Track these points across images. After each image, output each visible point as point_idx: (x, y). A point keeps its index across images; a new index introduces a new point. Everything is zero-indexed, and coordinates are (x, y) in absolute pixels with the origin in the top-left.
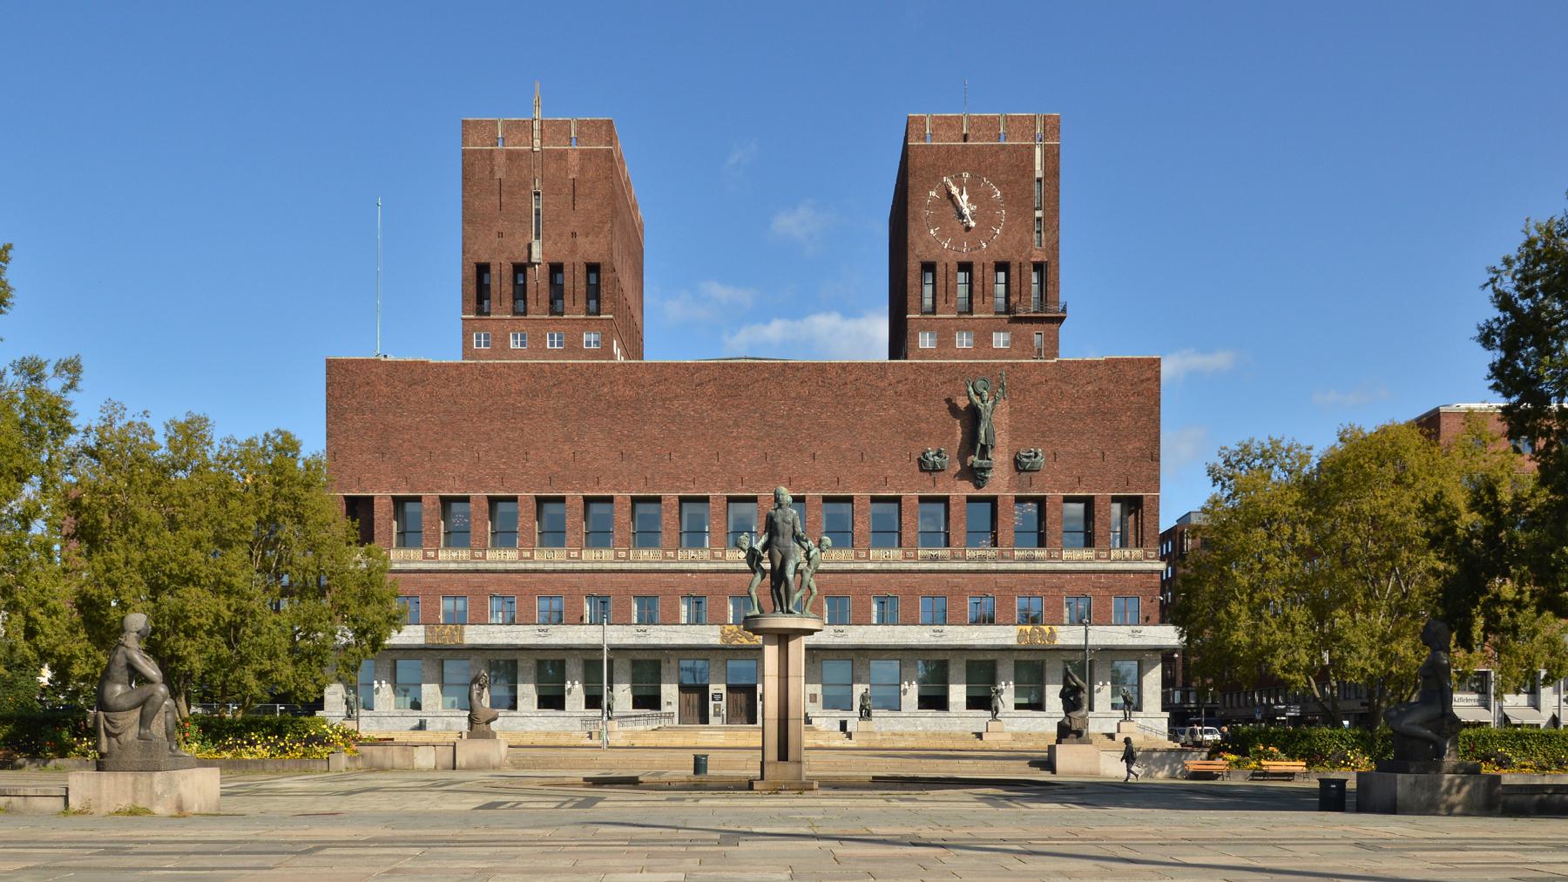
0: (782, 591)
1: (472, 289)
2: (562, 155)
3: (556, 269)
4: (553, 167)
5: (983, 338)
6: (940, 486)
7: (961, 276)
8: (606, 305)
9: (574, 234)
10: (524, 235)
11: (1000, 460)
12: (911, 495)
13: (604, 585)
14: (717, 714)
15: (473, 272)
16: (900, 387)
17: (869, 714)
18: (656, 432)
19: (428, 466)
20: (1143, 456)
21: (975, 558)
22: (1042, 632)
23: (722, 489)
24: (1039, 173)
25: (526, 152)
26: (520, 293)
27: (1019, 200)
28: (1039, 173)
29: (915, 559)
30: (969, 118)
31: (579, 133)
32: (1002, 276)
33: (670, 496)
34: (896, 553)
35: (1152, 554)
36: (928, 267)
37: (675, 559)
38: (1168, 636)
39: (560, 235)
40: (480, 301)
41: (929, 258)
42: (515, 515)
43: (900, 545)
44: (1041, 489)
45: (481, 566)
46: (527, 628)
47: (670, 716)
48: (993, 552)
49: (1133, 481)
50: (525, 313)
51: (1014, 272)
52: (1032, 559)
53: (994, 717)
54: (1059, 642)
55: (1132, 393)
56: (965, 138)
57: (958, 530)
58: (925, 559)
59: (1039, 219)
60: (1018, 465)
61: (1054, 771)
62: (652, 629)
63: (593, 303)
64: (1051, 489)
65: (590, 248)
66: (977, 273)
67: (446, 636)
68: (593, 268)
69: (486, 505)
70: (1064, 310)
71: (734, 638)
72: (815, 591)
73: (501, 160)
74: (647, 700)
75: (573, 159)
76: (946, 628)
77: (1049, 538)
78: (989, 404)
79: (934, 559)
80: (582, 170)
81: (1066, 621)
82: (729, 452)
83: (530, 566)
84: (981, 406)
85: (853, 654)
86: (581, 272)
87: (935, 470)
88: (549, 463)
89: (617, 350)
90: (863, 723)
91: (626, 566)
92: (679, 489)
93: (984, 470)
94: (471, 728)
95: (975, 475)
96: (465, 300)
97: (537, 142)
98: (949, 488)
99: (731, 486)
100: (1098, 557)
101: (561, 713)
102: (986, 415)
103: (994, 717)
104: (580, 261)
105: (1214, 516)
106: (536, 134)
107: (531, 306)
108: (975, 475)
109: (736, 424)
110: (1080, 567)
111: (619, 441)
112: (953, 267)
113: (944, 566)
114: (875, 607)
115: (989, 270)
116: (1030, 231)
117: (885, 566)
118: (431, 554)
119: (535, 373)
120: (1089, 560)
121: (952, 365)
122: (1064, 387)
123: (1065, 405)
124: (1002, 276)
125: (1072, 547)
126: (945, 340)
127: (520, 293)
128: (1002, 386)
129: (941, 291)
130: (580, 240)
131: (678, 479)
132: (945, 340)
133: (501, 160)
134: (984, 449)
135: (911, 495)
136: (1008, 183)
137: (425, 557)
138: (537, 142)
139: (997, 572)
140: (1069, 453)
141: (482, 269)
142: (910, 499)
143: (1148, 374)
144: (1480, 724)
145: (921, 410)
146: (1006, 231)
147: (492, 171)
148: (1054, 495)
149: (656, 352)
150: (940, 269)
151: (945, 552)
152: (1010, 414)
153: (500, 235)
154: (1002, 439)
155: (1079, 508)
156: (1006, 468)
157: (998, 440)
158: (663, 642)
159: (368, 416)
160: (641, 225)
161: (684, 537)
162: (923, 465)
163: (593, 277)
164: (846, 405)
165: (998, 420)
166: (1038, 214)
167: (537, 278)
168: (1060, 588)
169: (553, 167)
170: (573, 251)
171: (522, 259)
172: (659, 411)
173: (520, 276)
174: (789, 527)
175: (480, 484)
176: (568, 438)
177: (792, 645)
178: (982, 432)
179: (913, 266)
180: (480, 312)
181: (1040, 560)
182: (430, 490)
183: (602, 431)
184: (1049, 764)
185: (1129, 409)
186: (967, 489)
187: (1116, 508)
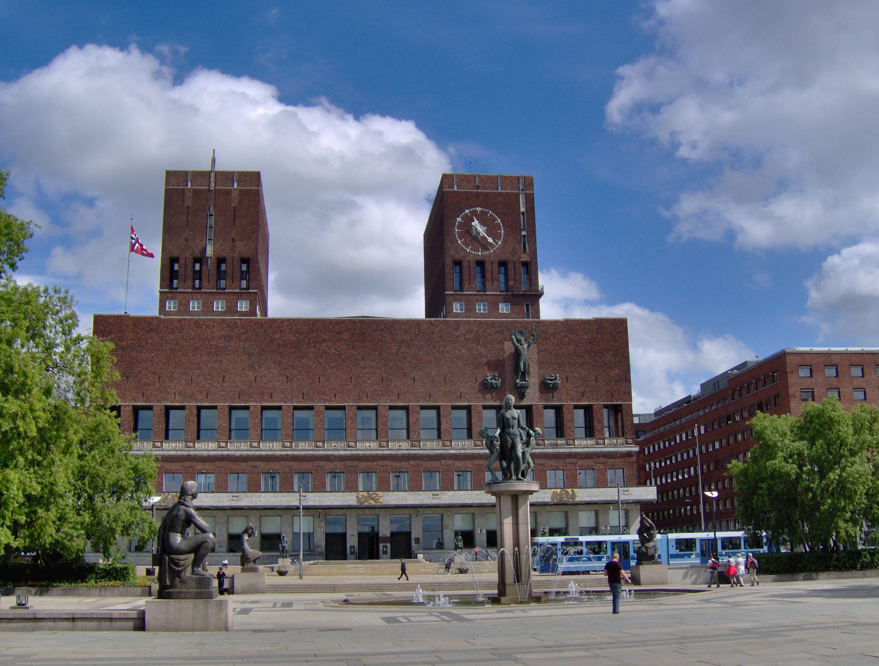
2: (228, 193)
5: (494, 307)
9: (233, 240)
10: (202, 240)
11: (533, 381)
14: (352, 553)
15: (168, 262)
16: (468, 336)
19: (158, 385)
22: (567, 492)
23: (353, 401)
24: (522, 209)
25: (204, 191)
27: (512, 226)
28: (522, 209)
30: (480, 176)
32: (502, 269)
36: (458, 263)
38: (649, 493)
39: (225, 240)
44: (560, 400)
46: (225, 495)
50: (200, 288)
51: (510, 266)
54: (577, 499)
56: (478, 187)
59: (524, 236)
70: (542, 288)
71: (365, 501)
72: (532, 465)
73: (189, 195)
75: (235, 195)
78: (526, 346)
81: (469, 487)
82: (359, 377)
85: (280, 512)
88: (239, 384)
89: (258, 312)
92: (325, 401)
95: (520, 393)
97: (213, 184)
99: (360, 400)
104: (236, 255)
106: (212, 179)
107: (205, 284)
109: (363, 359)
112: (473, 264)
114: (456, 478)
115: (495, 266)
116: (519, 243)
118: (223, 444)
119: (232, 325)
121: (500, 322)
122: (570, 336)
123: (571, 347)
126: (470, 309)
128: (533, 335)
130: (237, 243)
131: (324, 393)
132: (470, 309)
133: (189, 195)
134: (523, 374)
138: (213, 184)
141: (174, 260)
142: (477, 406)
145: (482, 350)
146: (504, 242)
147: (183, 202)
148: (568, 403)
149: (272, 313)
152: (538, 353)
153: (187, 240)
154: (534, 369)
155: (433, 413)
156: (537, 387)
157: (531, 369)
158: (317, 504)
161: (233, 433)
164: (434, 347)
166: (524, 233)
172: (313, 350)
175: (192, 397)
176: (251, 367)
178: (522, 364)
182: (159, 401)
183: (275, 363)
185: (610, 350)
187: (605, 411)
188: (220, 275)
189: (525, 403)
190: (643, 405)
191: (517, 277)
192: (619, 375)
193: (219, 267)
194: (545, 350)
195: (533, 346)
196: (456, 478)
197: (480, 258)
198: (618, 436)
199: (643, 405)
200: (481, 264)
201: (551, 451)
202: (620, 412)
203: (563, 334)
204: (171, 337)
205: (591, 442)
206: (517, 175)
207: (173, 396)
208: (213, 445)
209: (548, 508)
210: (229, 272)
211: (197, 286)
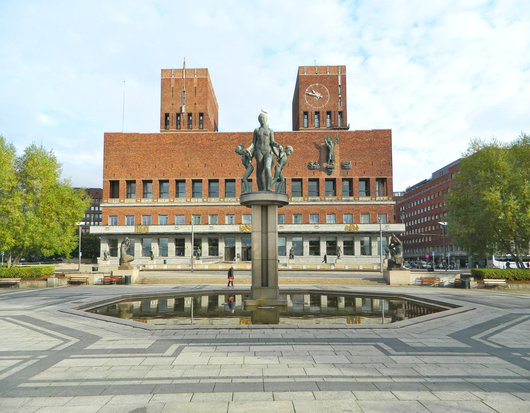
0: (263, 176)
1: (164, 121)
2: (192, 80)
3: (190, 115)
4: (189, 83)
6: (316, 175)
7: (316, 116)
8: (205, 126)
11: (337, 165)
12: (306, 178)
13: (199, 211)
14: (238, 257)
16: (301, 140)
17: (293, 257)
18: (217, 156)
20: (386, 164)
21: (329, 200)
22: (354, 226)
26: (178, 123)
27: (334, 93)
28: (340, 84)
29: (308, 201)
31: (197, 73)
32: (328, 116)
33: (222, 179)
34: (301, 199)
35: (391, 199)
36: (306, 113)
37: (224, 201)
38: (401, 228)
40: (166, 125)
41: (305, 110)
42: (168, 187)
43: (302, 196)
44: (351, 176)
45: (156, 205)
47: (221, 258)
48: (335, 198)
49: (383, 172)
51: (333, 114)
52: (349, 201)
53: (339, 257)
55: (380, 142)
57: (322, 191)
58: (311, 201)
59: (340, 98)
60: (343, 167)
61: (388, 283)
62: (215, 226)
63: (201, 125)
64: (355, 176)
65: (200, 108)
66: (321, 115)
67: (142, 230)
68: (201, 114)
69: (158, 183)
73: (173, 81)
74: (180, 252)
75: (195, 81)
76: (320, 225)
77: (355, 193)
78: (333, 146)
79: (314, 201)
80: (198, 84)
83: (173, 204)
84: (330, 146)
86: (197, 115)
87: (314, 169)
88: (180, 168)
90: (290, 260)
91: (206, 204)
93: (331, 169)
94: (120, 265)
95: (329, 170)
96: (161, 125)
97: (184, 76)
98: (319, 176)
100: (372, 199)
101: (183, 257)
102: (332, 149)
103: (339, 257)
105: (488, 151)
107: (182, 127)
108: (329, 170)
110: (365, 203)
111: (204, 160)
112: (314, 113)
113: (318, 203)
114: (293, 218)
115: (325, 114)
117: (297, 203)
120: (369, 201)
122: (358, 140)
123: (359, 146)
124: (328, 116)
125: (363, 196)
127: (178, 123)
129: (310, 120)
130: (197, 106)
131: (225, 173)
133: (173, 81)
134: (331, 161)
135: (306, 178)
136: (331, 87)
137: (137, 201)
138: (184, 76)
139: (336, 205)
140: (360, 163)
141: (167, 115)
142: (305, 179)
143: (388, 135)
144: (498, 260)
146: (330, 101)
147: (170, 85)
148: (356, 178)
150: (309, 114)
151: (317, 198)
153: (173, 104)
154: (337, 158)
156: (339, 168)
157: (336, 159)
159: (118, 152)
160: (217, 105)
162: (310, 167)
163: (201, 118)
165: (335, 150)
166: (340, 96)
167: (184, 118)
168: (359, 211)
169: (189, 83)
170: (195, 109)
171: (179, 112)
173: (179, 118)
174: (268, 138)
175: (156, 175)
177: (270, 211)
179: (301, 112)
180: (166, 128)
181: (351, 201)
182: (139, 178)
184: (386, 281)
186: (324, 176)
188: (190, 122)
189: (332, 177)
190: (401, 184)
191: (336, 120)
192: (385, 161)
193: (189, 118)
194: (344, 148)
195: (337, 145)
196: (293, 218)
197: (317, 110)
198: (384, 195)
199: (401, 184)
200: (317, 113)
201: (345, 203)
202: (385, 182)
203: (354, 138)
204: (145, 144)
205: (368, 198)
206: (337, 65)
207: (146, 175)
208: (167, 200)
209: (343, 235)
210: (193, 120)
211: (201, 127)
